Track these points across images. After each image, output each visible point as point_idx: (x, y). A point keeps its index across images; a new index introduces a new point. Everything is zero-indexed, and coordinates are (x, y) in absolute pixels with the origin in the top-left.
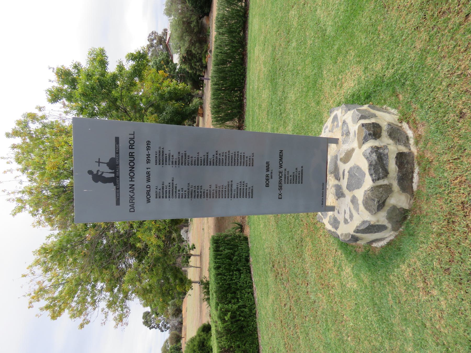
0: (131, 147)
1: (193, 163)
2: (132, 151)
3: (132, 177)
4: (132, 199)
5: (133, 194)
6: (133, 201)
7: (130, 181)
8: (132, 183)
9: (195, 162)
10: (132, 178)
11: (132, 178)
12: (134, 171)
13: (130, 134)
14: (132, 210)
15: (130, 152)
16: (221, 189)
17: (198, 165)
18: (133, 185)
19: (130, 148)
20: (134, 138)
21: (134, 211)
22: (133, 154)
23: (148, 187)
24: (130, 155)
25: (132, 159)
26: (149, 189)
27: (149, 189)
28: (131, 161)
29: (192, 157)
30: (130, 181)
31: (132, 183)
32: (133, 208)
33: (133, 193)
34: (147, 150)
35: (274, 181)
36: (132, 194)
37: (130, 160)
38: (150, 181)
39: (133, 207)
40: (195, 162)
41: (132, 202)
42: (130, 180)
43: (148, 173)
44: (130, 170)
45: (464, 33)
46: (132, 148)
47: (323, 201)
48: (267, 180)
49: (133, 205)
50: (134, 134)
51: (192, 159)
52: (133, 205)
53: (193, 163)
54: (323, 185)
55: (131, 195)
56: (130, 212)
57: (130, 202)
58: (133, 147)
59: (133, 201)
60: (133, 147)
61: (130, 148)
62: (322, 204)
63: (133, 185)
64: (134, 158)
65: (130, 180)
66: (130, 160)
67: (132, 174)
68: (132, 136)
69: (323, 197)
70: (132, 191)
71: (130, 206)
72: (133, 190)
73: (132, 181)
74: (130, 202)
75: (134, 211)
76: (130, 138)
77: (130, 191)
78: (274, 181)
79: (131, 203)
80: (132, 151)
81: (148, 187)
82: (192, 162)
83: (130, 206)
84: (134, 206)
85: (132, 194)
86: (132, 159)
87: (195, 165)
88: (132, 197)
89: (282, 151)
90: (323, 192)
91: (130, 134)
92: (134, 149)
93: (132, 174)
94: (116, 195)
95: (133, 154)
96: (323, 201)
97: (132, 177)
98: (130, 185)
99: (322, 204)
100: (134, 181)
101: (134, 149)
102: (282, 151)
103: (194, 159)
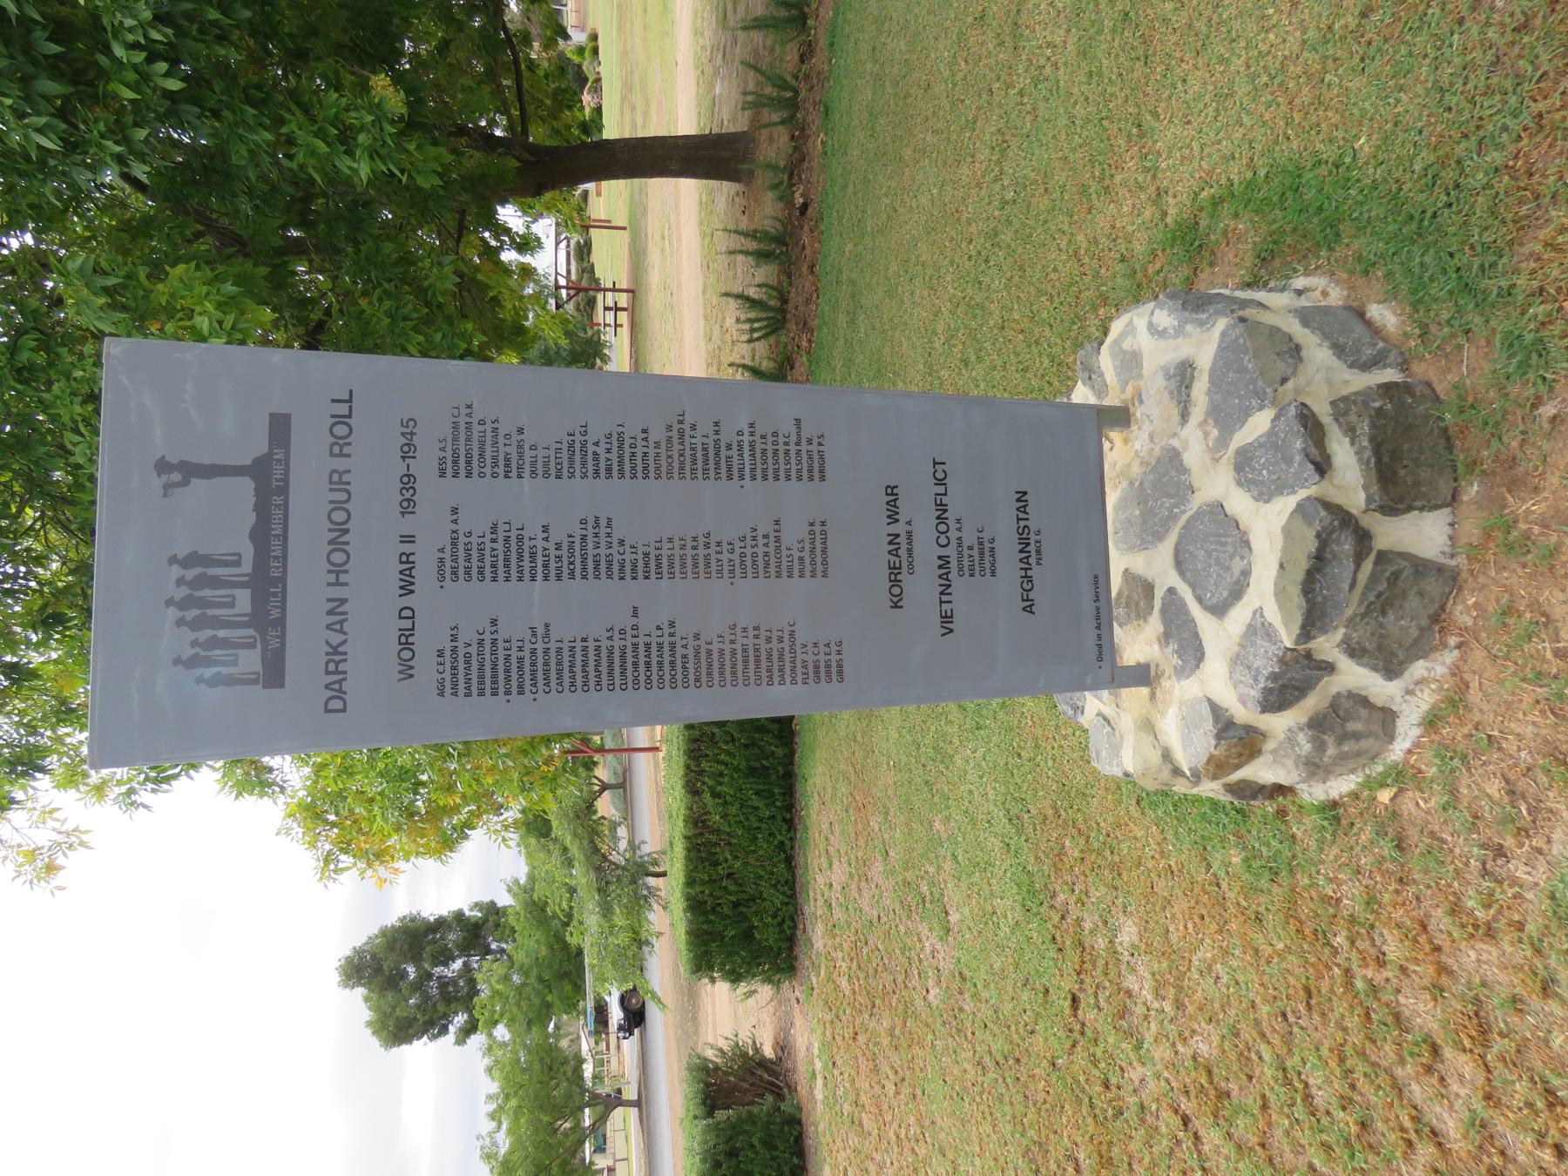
0: (336, 450)
1: (540, 471)
2: (340, 464)
3: (338, 570)
4: (337, 658)
5: (344, 637)
6: (342, 667)
7: (329, 584)
8: (338, 592)
9: (546, 464)
10: (338, 573)
11: (338, 573)
12: (347, 543)
13: (333, 401)
14: (337, 704)
15: (336, 471)
16: (727, 647)
17: (559, 477)
18: (344, 601)
19: (332, 455)
20: (350, 416)
21: (344, 710)
22: (345, 478)
23: (407, 613)
24: (331, 482)
25: (343, 496)
26: (407, 624)
27: (407, 624)
28: (338, 506)
29: (533, 447)
30: (329, 584)
31: (338, 592)
32: (340, 694)
33: (341, 631)
34: (403, 458)
35: (921, 585)
36: (336, 639)
37: (331, 502)
38: (412, 592)
39: (340, 690)
40: (546, 464)
41: (337, 672)
42: (332, 578)
43: (404, 558)
44: (331, 542)
45: (1139, 126)
46: (341, 455)
47: (1100, 646)
48: (895, 582)
49: (340, 682)
50: (350, 401)
51: (533, 453)
52: (340, 682)
53: (540, 471)
54: (1096, 583)
55: (334, 643)
56: (327, 711)
57: (328, 673)
58: (346, 450)
59: (342, 667)
60: (346, 450)
61: (332, 455)
62: (1100, 658)
63: (344, 601)
64: (348, 492)
65: (332, 578)
66: (331, 502)
67: (338, 557)
68: (343, 409)
69: (1098, 628)
70: (338, 627)
71: (327, 687)
72: (341, 622)
73: (337, 584)
74: (328, 673)
75: (344, 710)
76: (333, 416)
77: (328, 627)
78: (921, 585)
79: (336, 483)
80: (340, 464)
81: (407, 613)
82: (534, 464)
83: (327, 687)
84: (345, 686)
85: (336, 639)
86: (343, 496)
87: (546, 475)
88: (335, 650)
89: (1025, 493)
90: (1098, 609)
91: (333, 401)
92: (349, 456)
93: (338, 557)
94: (284, 602)
95: (345, 478)
96: (1100, 646)
97: (338, 570)
98: (329, 600)
99: (1100, 658)
100: (346, 584)
101: (349, 456)
102: (1025, 493)
103: (541, 453)
